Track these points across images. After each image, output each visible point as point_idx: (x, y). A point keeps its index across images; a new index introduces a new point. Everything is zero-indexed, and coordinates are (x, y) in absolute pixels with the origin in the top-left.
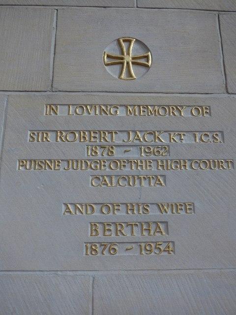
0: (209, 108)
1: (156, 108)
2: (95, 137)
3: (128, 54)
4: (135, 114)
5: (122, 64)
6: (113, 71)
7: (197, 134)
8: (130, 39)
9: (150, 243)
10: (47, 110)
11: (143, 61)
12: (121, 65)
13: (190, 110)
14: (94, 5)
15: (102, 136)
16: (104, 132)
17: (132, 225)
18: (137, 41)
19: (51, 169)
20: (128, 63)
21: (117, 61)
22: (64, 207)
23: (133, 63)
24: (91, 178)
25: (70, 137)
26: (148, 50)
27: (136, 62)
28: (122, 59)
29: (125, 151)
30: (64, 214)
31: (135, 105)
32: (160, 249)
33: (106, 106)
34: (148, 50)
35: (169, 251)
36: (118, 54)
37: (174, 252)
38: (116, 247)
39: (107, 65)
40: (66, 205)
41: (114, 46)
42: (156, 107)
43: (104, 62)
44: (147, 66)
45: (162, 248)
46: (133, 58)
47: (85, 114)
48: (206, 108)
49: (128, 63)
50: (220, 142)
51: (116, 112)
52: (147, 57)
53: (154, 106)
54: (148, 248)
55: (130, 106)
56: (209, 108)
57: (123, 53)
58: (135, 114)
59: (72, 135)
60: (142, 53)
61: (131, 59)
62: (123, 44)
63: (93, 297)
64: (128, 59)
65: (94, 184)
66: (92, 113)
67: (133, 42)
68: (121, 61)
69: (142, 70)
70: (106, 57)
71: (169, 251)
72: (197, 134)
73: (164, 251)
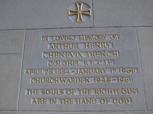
1: (94, 37)
2: (93, 46)
4: (84, 39)
5: (77, 14)
8: (80, 3)
9: (99, 78)
11: (87, 13)
12: (76, 16)
13: (110, 37)
14: (104, 27)
15: (103, 45)
16: (104, 43)
19: (100, 47)
20: (80, 14)
21: (75, 13)
22: (32, 100)
23: (82, 14)
24: (31, 79)
26: (90, 7)
27: (83, 13)
30: (33, 103)
34: (90, 7)
36: (74, 10)
39: (69, 16)
41: (73, 6)
42: (94, 36)
44: (89, 16)
48: (88, 36)
49: (80, 14)
50: (137, 72)
52: (89, 11)
55: (82, 35)
60: (86, 9)
62: (78, 6)
64: (80, 12)
65: (33, 82)
68: (77, 13)
69: (87, 17)
70: (69, 11)
71: (104, 81)
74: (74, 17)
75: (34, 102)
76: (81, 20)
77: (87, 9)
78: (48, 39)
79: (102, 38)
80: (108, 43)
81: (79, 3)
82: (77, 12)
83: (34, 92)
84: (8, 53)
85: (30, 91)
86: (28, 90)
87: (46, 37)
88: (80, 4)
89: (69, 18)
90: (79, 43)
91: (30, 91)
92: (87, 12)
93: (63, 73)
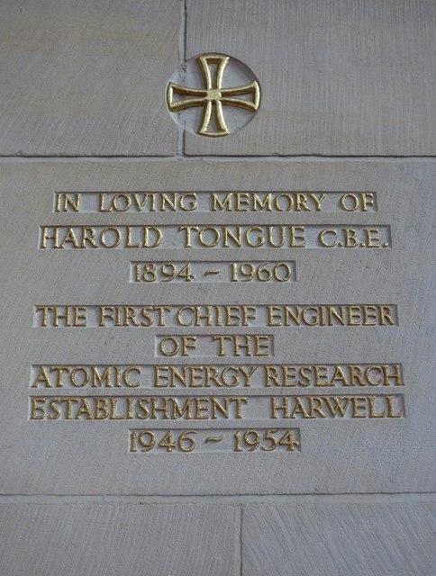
0: (373, 196)
3: (215, 86)
4: (228, 210)
5: (204, 104)
6: (185, 121)
7: (235, 265)
10: (57, 204)
11: (244, 100)
16: (301, 196)
17: (236, 400)
18: (233, 61)
20: (214, 103)
21: (192, 100)
22: (33, 372)
23: (224, 103)
25: (205, 238)
27: (227, 101)
28: (204, 95)
29: (206, 274)
30: (34, 386)
31: (227, 192)
32: (273, 440)
33: (172, 194)
35: (290, 445)
36: (191, 85)
37: (298, 447)
38: (190, 436)
39: (172, 110)
40: (39, 367)
43: (258, 83)
44: (252, 110)
45: (276, 438)
46: (224, 94)
47: (131, 210)
49: (214, 103)
51: (192, 204)
52: (252, 91)
53: (267, 193)
54: (249, 440)
56: (373, 196)
57: (206, 86)
58: (228, 210)
59: (209, 234)
60: (239, 84)
61: (220, 94)
63: (11, 495)
64: (214, 95)
66: (144, 209)
67: (224, 65)
69: (241, 117)
70: (171, 90)
72: (235, 265)
73: (280, 444)
74: (190, 115)
75: (38, 380)
76: (219, 128)
77: (241, 84)
78: (79, 206)
79: (301, 205)
80: (313, 195)
81: (222, 134)
82: (205, 95)
83: (64, 318)
84: (68, 153)
85: (48, 316)
86: (40, 309)
87: (69, 197)
88: (216, 63)
89: (169, 117)
90: (198, 335)
91: (48, 316)
92: (243, 97)
93: (146, 277)
